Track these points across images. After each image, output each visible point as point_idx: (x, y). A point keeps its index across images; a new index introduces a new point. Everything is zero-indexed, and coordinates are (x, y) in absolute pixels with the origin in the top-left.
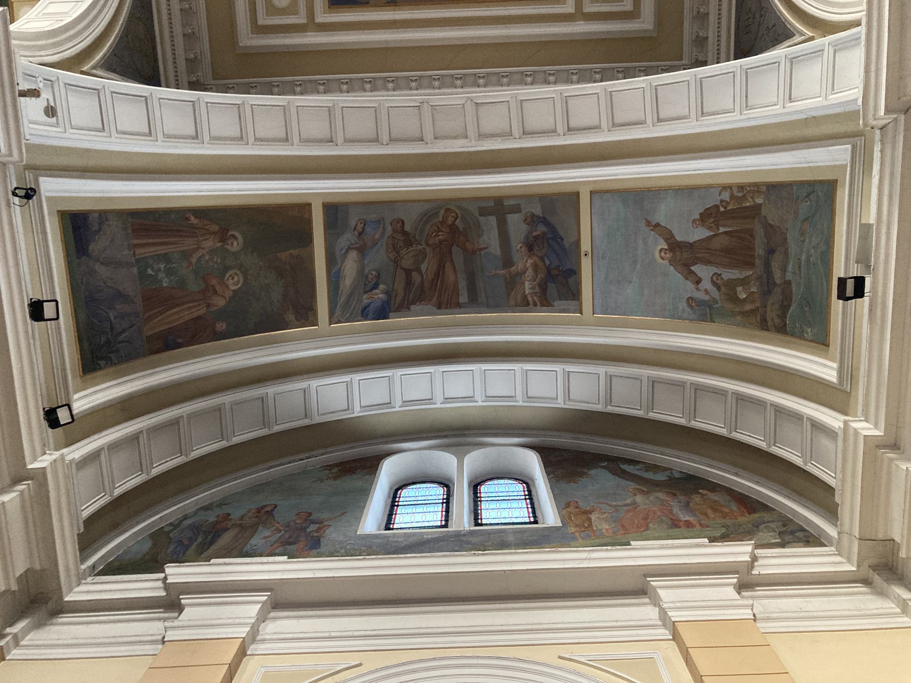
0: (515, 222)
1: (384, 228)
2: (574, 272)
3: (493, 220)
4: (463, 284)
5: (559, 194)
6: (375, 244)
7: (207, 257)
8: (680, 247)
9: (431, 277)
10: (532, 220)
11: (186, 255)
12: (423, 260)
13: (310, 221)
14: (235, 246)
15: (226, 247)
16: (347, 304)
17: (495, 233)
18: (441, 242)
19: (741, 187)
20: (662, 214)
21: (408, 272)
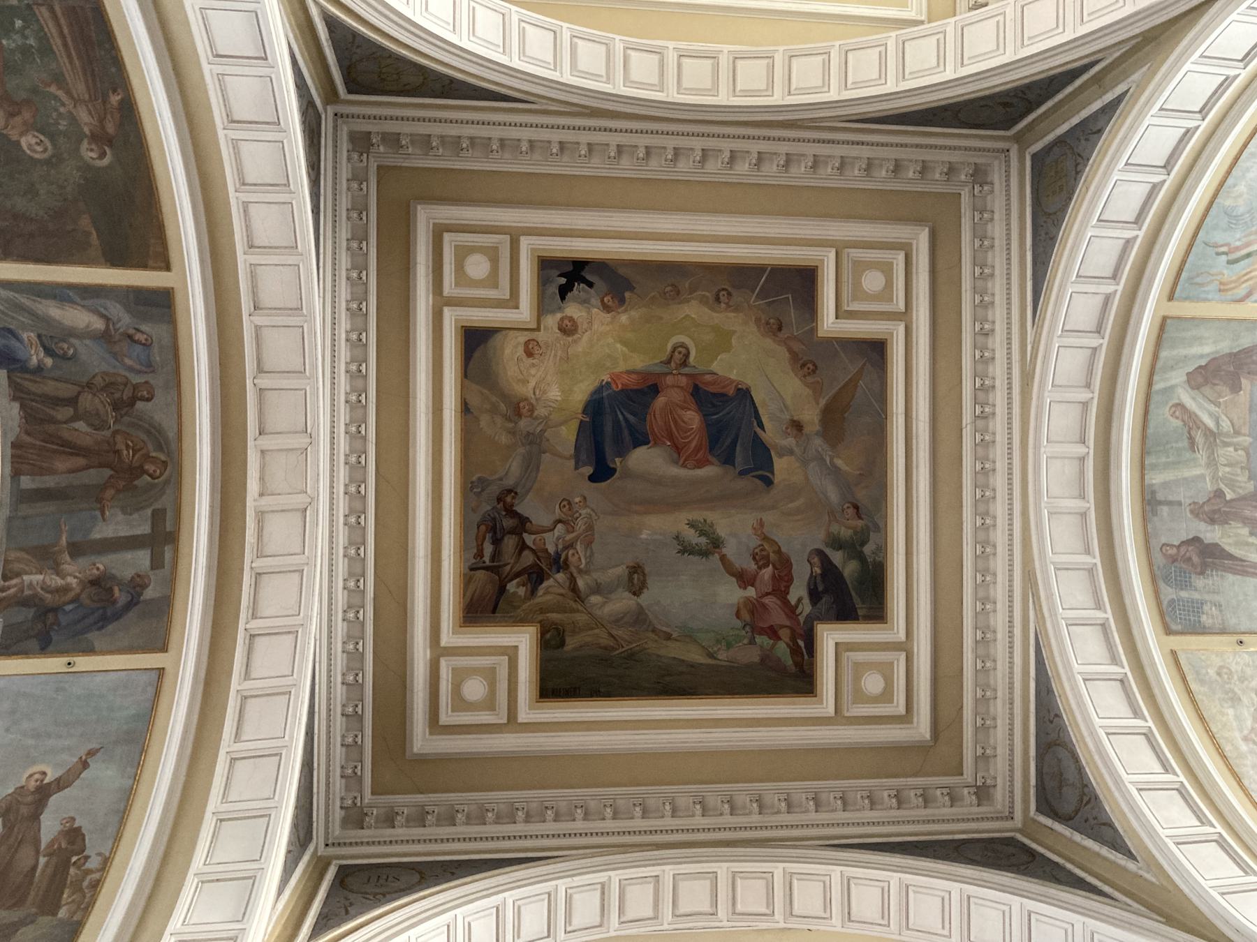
0: (142, 559)
1: (140, 372)
2: (45, 647)
3: (145, 529)
4: (49, 482)
5: (170, 621)
6: (115, 355)
7: (62, 110)
8: (40, 800)
9: (66, 435)
10: (137, 585)
11: (58, 79)
12: (91, 425)
13: (144, 266)
14: (89, 153)
15: (85, 142)
16: (21, 308)
17: (124, 532)
18: (118, 452)
19: (96, 885)
20: (104, 774)
21: (73, 401)
